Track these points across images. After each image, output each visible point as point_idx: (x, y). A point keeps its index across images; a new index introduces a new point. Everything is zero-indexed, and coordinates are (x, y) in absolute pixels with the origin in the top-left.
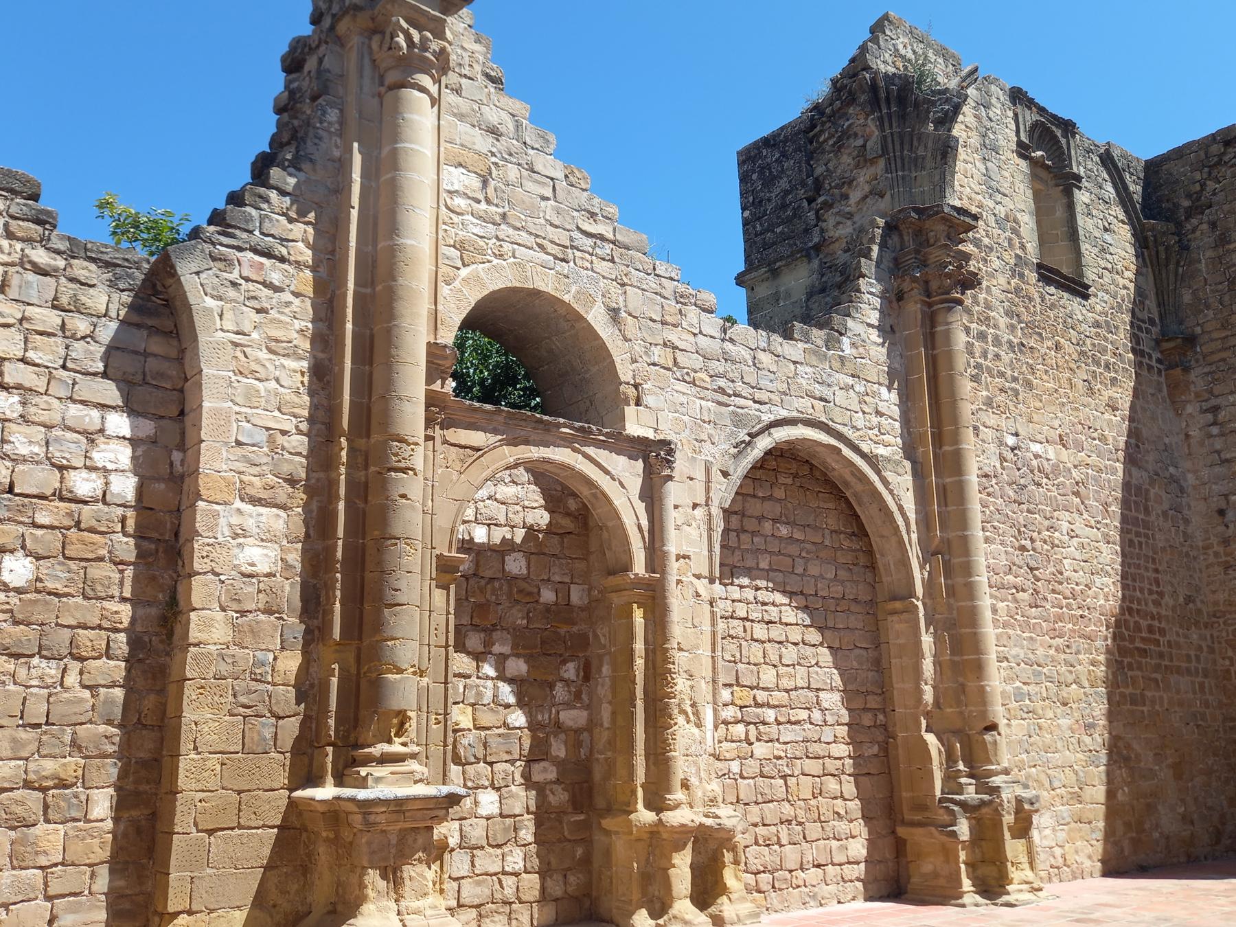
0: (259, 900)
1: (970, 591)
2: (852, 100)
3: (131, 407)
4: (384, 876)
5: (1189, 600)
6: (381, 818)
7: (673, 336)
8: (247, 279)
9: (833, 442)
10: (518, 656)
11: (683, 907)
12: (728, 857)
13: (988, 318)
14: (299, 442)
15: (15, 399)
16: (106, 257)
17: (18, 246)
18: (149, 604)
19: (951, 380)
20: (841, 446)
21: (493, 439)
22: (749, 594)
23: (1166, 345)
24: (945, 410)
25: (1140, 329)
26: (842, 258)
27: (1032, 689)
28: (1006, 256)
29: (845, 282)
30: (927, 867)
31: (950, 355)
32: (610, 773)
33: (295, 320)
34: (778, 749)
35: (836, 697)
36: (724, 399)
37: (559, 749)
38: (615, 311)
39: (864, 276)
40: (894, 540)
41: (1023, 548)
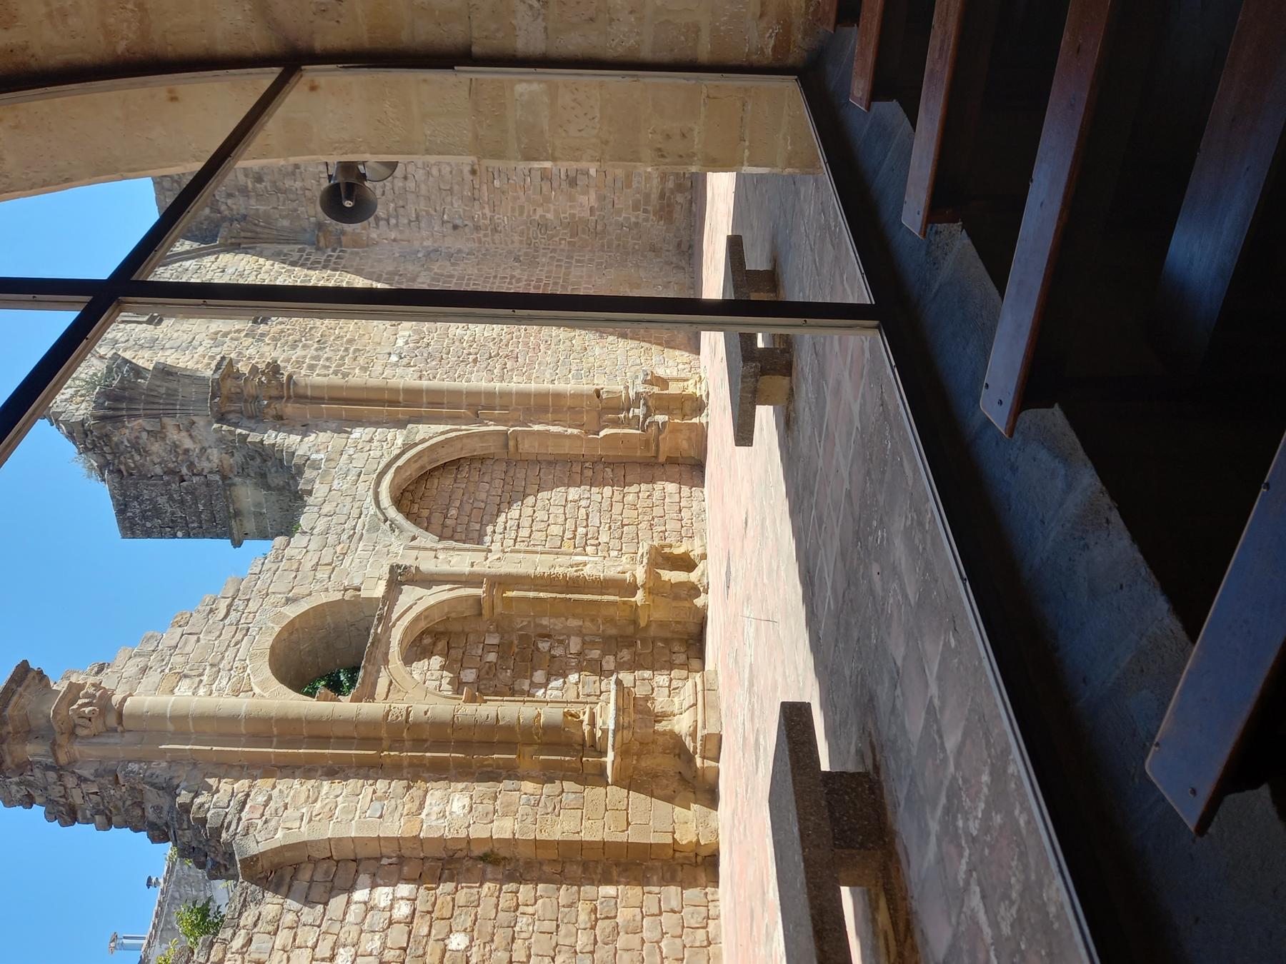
0: (669, 799)
1: (505, 395)
2: (106, 437)
3: (351, 889)
4: (660, 722)
5: (517, 259)
6: (626, 720)
7: (308, 565)
8: (262, 815)
9: (392, 470)
10: (532, 675)
11: (693, 576)
12: (667, 550)
13: (298, 362)
14: (381, 785)
15: (341, 950)
16: (239, 906)
17: (229, 955)
18: (484, 872)
19: (349, 388)
20: (395, 466)
21: (383, 673)
22: (498, 537)
23: (322, 244)
24: (373, 396)
25: (307, 259)
26: (238, 458)
27: (574, 367)
28: (246, 344)
29: (260, 454)
30: (685, 445)
31: (331, 387)
32: (611, 621)
33: (294, 789)
34: (605, 528)
35: (572, 490)
36: (357, 536)
37: (595, 654)
38: (288, 600)
39: (262, 441)
40: (465, 441)
41: (475, 361)
